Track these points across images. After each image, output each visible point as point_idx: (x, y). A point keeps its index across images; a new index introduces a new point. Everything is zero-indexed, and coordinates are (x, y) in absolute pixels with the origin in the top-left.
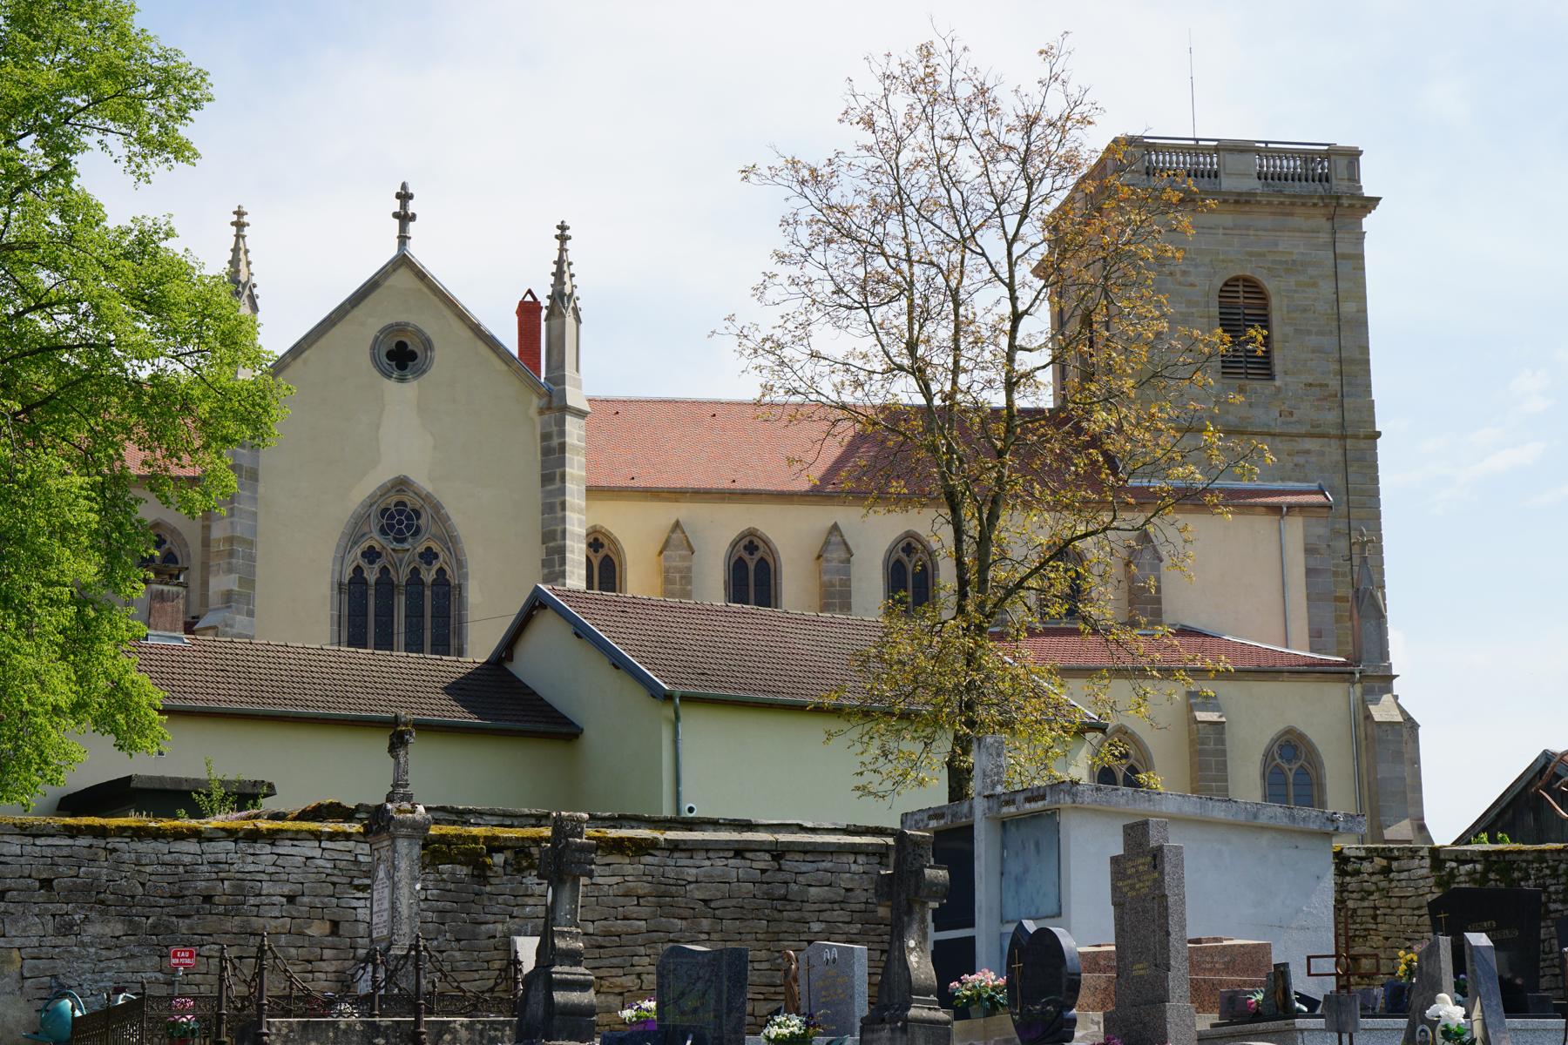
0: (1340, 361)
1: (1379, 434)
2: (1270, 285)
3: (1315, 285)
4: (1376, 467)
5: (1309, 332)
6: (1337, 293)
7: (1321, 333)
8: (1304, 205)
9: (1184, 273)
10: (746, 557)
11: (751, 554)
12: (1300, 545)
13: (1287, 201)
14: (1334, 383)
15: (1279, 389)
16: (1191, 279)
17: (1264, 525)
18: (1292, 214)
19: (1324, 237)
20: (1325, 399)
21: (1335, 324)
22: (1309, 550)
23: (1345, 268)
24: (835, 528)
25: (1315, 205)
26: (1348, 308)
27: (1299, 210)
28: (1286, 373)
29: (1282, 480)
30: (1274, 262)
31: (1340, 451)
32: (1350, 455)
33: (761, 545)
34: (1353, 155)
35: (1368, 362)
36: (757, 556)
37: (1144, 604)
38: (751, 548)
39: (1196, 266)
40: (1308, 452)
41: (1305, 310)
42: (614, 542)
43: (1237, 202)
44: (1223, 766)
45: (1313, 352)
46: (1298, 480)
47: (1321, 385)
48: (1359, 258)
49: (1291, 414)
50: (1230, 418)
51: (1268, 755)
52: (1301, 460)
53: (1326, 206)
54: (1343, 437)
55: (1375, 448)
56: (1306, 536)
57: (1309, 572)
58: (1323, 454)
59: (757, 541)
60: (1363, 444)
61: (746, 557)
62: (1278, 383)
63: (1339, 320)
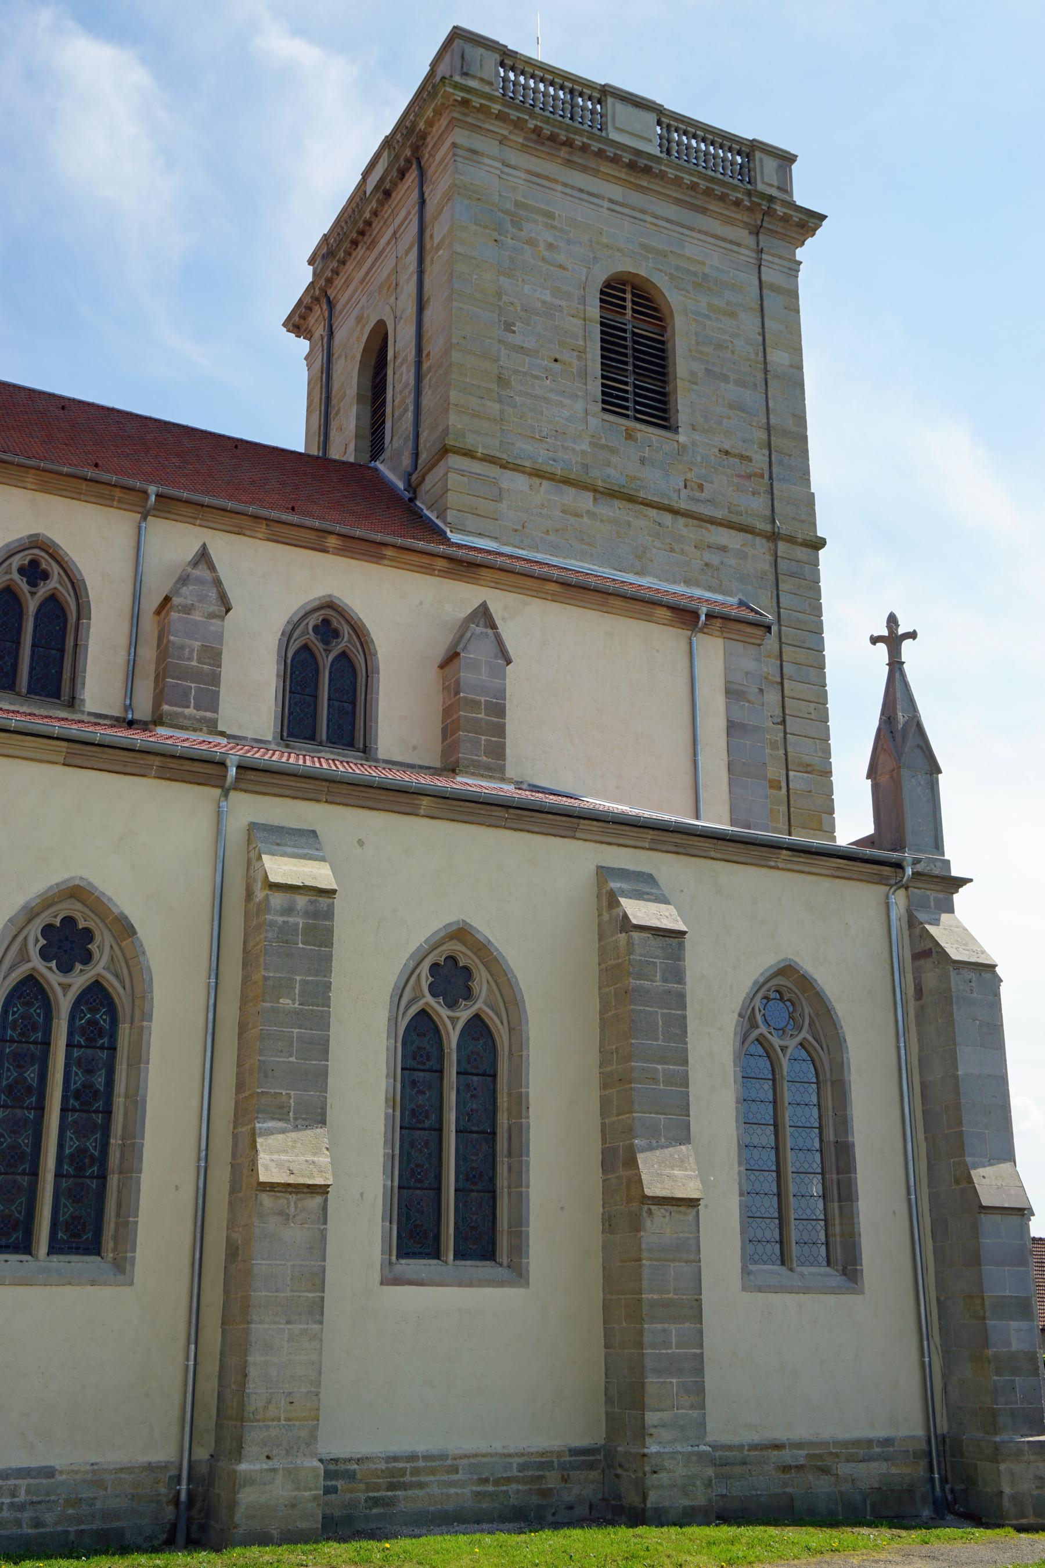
0: (768, 429)
1: (821, 543)
2: (674, 298)
3: (733, 315)
4: (818, 591)
5: (725, 378)
6: (763, 334)
7: (741, 383)
8: (723, 198)
9: (551, 246)
10: (318, 646)
11: (33, 583)
12: (720, 683)
13: (703, 184)
14: (760, 459)
15: (682, 450)
16: (561, 258)
17: (665, 641)
18: (703, 211)
19: (748, 255)
20: (749, 477)
21: (760, 375)
22: (733, 693)
23: (772, 302)
24: (484, 606)
25: (737, 203)
26: (778, 358)
27: (714, 206)
28: (694, 428)
29: (688, 582)
30: (678, 268)
31: (769, 558)
32: (782, 565)
33: (346, 629)
34: (787, 159)
35: (805, 439)
36: (43, 590)
37: (470, 721)
38: (327, 631)
39: (569, 242)
40: (723, 549)
41: (719, 346)
42: (359, 631)
43: (632, 166)
44: (681, 1025)
45: (731, 407)
46: (710, 589)
47: (741, 457)
48: (793, 294)
49: (701, 487)
50: (612, 471)
51: (749, 1020)
52: (714, 558)
53: (750, 210)
54: (774, 537)
55: (816, 564)
56: (727, 670)
57: (733, 727)
58: (745, 557)
59: (47, 563)
60: (801, 553)
61: (318, 646)
62: (682, 438)
63: (766, 371)
